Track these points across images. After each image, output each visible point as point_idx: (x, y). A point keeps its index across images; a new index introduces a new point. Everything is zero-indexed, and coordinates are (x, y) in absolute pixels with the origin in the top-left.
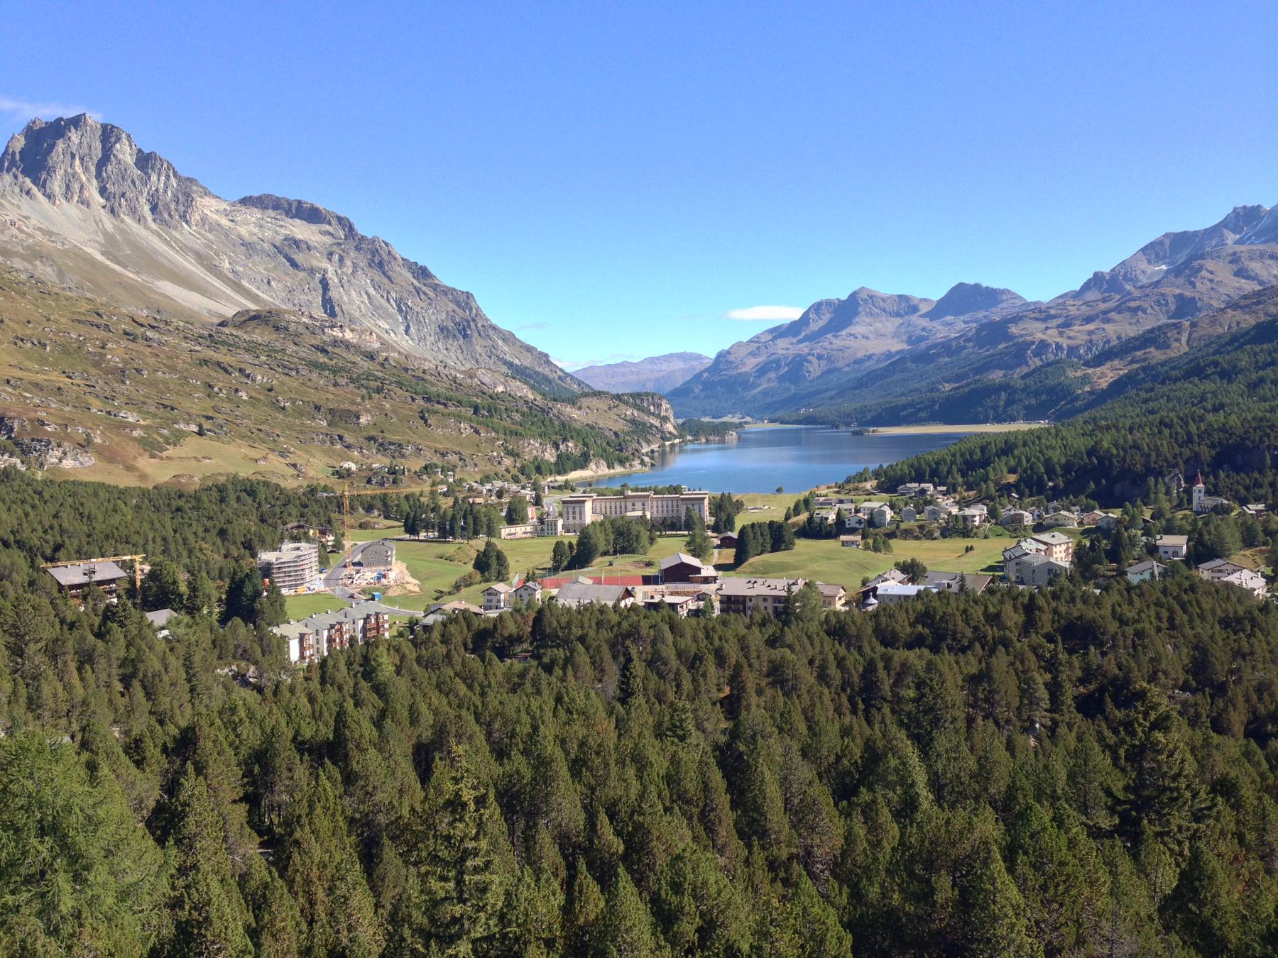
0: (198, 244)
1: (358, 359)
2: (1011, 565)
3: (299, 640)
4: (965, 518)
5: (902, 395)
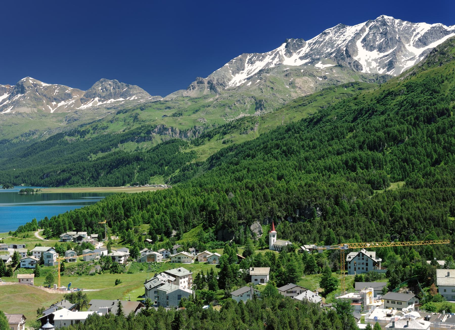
1: (101, 160)
2: (151, 293)
4: (114, 258)
5: (59, 162)
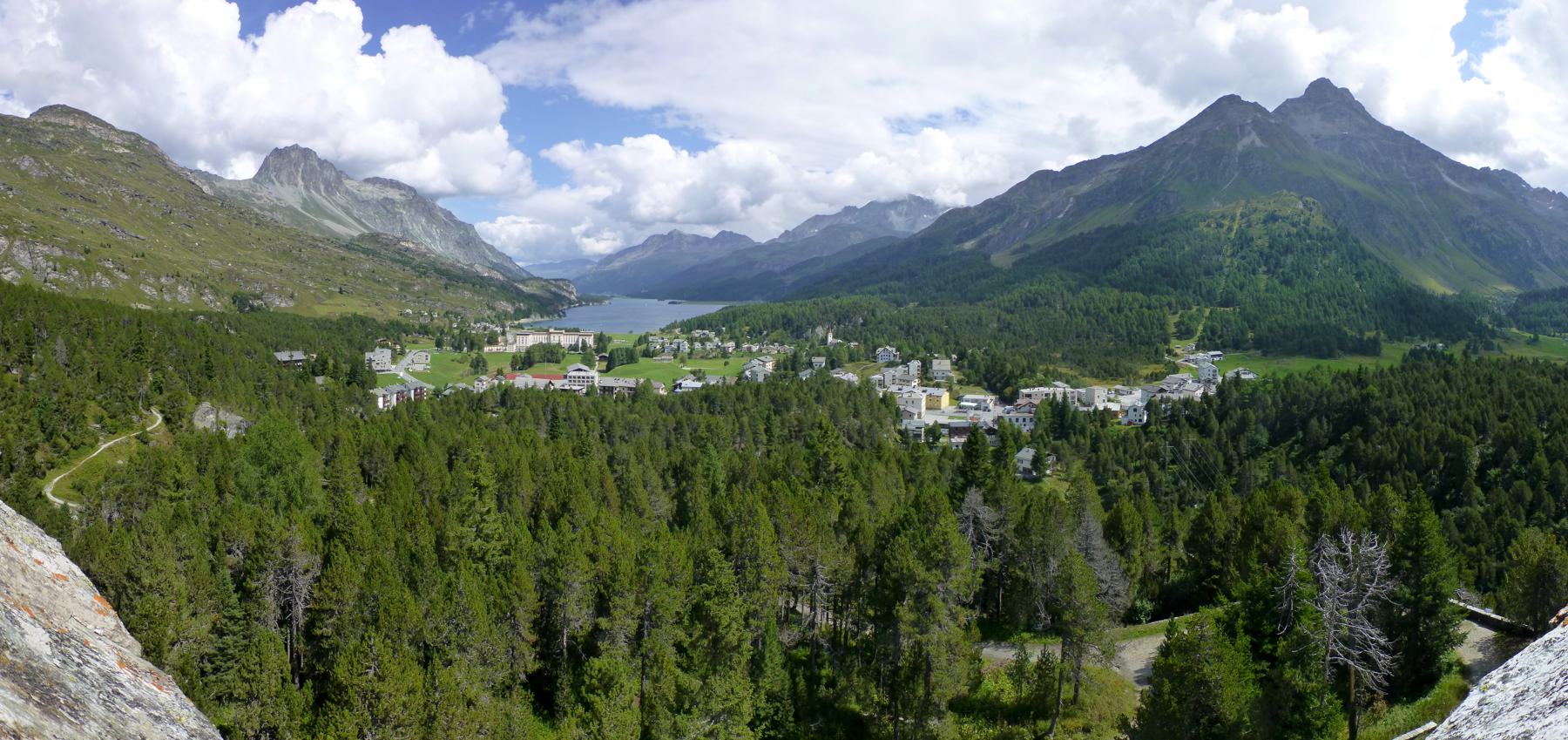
0: (343, 202)
3: (384, 400)
